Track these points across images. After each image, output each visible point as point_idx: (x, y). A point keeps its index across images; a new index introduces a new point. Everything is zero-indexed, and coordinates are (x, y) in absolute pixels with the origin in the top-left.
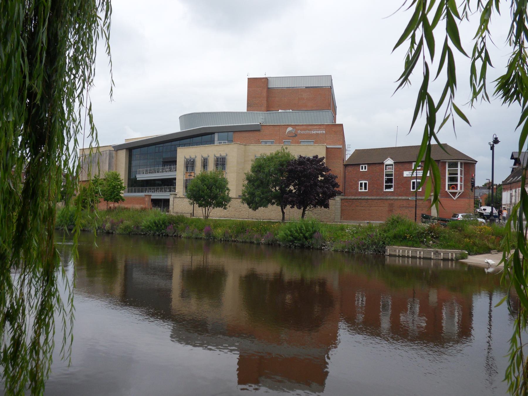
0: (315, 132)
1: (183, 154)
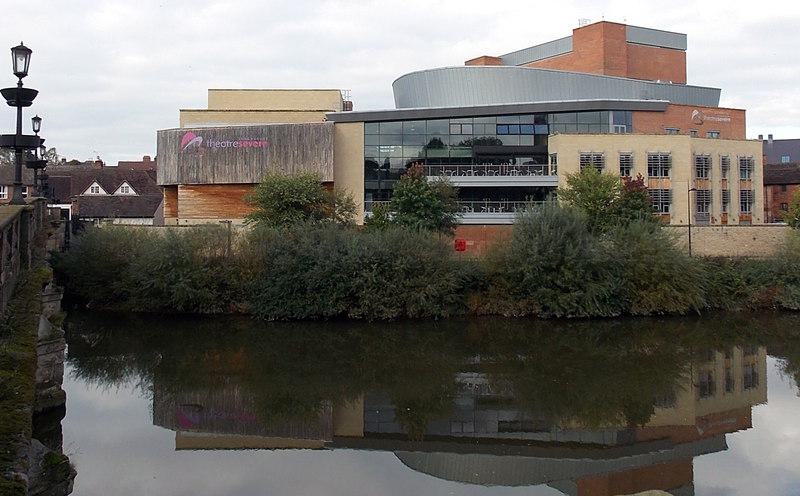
0: (720, 120)
1: (567, 150)
